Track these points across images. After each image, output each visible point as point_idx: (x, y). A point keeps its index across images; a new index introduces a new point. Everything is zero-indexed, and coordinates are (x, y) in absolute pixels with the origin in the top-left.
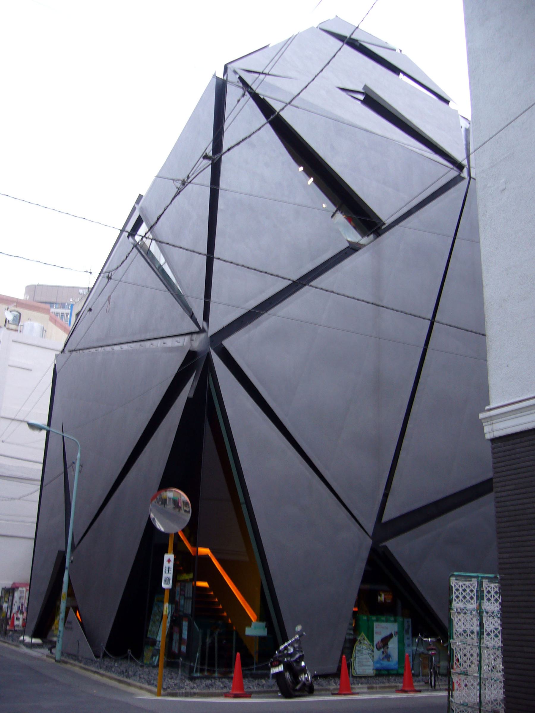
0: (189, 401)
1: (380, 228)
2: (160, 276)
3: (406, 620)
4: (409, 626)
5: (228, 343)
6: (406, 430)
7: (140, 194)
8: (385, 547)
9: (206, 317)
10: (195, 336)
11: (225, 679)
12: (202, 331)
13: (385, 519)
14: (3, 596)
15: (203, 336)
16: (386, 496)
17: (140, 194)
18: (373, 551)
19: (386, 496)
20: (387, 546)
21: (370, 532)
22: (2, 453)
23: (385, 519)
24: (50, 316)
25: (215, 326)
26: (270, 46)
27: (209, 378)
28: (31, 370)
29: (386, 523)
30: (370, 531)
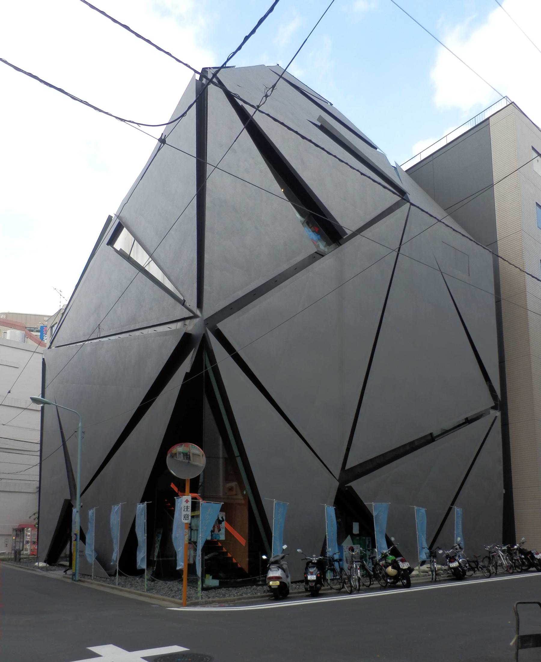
0: (187, 375)
1: (341, 237)
2: (304, 92)
3: (367, 538)
4: (369, 542)
5: (224, 326)
6: (363, 402)
7: (109, 215)
8: (350, 487)
9: (200, 305)
10: (188, 322)
11: (62, 567)
12: (195, 316)
13: (347, 467)
14: (433, 570)
15: (196, 321)
16: (348, 450)
17: (109, 215)
18: (339, 490)
19: (348, 450)
20: (352, 486)
21: (337, 477)
22: (1, 437)
23: (347, 467)
24: (26, 332)
25: (210, 308)
26: (235, 67)
27: (205, 358)
28: (18, 368)
29: (348, 470)
30: (337, 476)
